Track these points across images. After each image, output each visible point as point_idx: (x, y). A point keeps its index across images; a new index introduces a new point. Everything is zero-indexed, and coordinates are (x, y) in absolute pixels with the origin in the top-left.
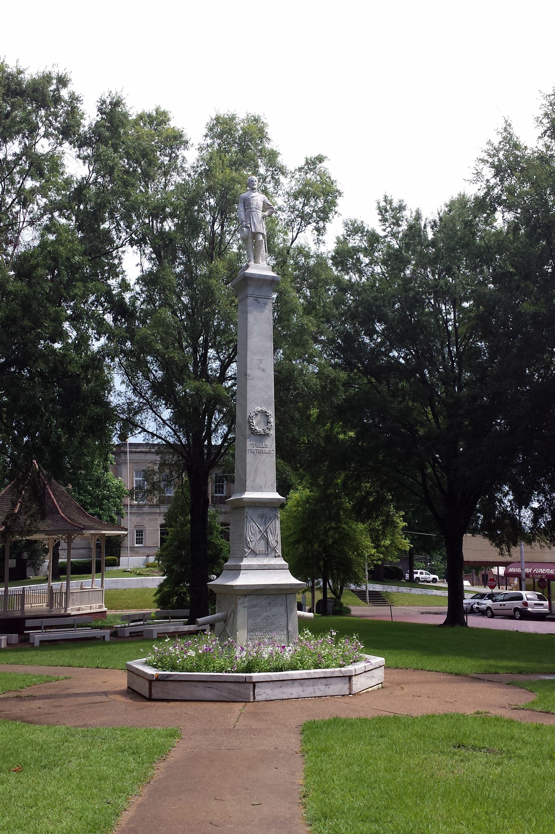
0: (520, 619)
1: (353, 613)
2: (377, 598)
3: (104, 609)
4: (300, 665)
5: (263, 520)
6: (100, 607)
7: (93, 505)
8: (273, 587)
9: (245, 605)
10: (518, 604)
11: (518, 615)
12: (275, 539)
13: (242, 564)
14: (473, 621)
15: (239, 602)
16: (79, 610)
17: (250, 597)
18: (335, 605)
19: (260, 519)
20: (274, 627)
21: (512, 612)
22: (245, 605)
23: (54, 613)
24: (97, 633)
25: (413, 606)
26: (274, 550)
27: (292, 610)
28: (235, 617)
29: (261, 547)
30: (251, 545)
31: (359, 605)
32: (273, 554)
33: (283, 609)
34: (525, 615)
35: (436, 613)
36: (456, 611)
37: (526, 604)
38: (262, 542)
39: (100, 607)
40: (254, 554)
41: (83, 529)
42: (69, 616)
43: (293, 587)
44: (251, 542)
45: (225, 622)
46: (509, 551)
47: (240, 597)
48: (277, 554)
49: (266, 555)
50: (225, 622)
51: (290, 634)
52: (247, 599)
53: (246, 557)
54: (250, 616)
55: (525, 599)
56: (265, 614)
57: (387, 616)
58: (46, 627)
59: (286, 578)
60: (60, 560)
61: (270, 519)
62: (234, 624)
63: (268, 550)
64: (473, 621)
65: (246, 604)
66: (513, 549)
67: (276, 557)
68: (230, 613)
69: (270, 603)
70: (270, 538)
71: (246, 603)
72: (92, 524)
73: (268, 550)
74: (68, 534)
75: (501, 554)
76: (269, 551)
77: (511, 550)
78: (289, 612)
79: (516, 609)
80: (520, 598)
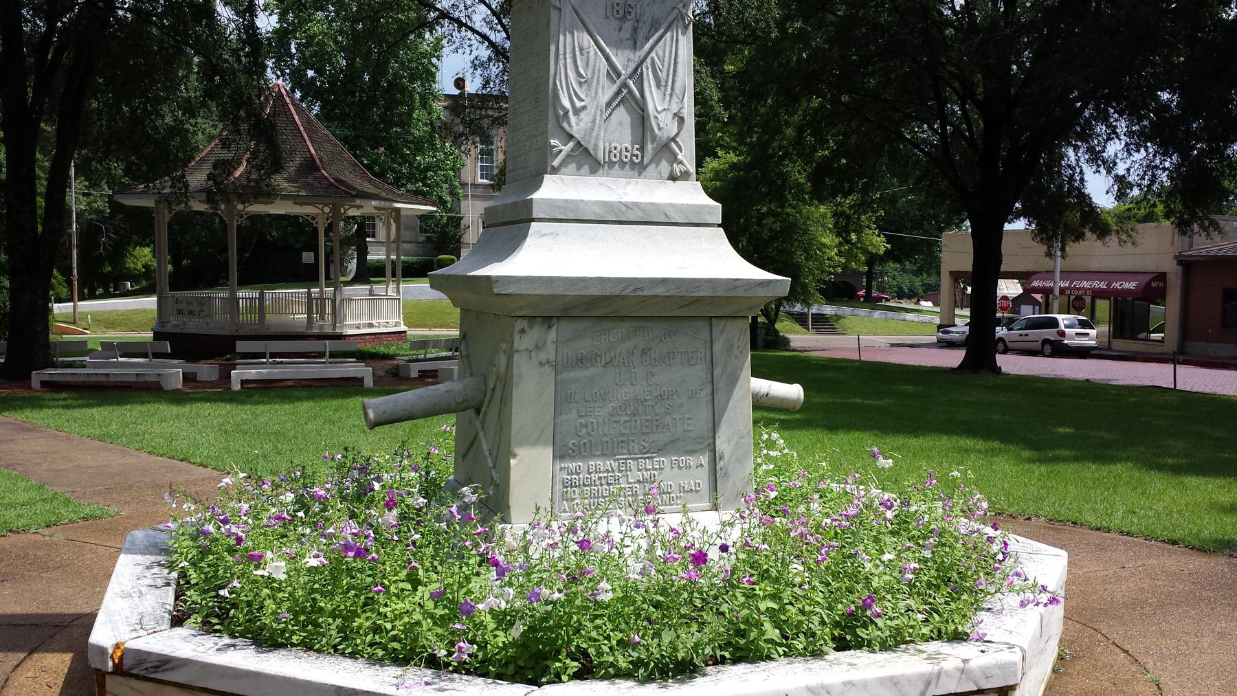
0: (1051, 356)
1: (793, 345)
2: (822, 323)
3: (403, 328)
4: (773, 634)
5: (628, 26)
6: (397, 324)
7: (411, 178)
8: (660, 291)
9: (543, 356)
10: (1050, 334)
11: (1048, 349)
12: (673, 103)
13: (536, 196)
14: (1009, 364)
15: (523, 343)
16: (371, 325)
17: (567, 328)
18: (767, 334)
19: (614, 24)
20: (662, 438)
21: (1038, 346)
22: (543, 356)
23: (316, 331)
24: (351, 368)
25: (875, 334)
26: (666, 149)
27: (733, 381)
28: (505, 401)
29: (616, 134)
30: (577, 125)
31: (797, 333)
32: (664, 167)
33: (697, 373)
34: (1059, 350)
35: (912, 346)
36: (981, 346)
37: (1062, 334)
38: (622, 115)
39: (397, 324)
40: (587, 159)
41: (356, 196)
42: (341, 337)
43: (739, 293)
44: (577, 111)
45: (478, 411)
46: (1063, 250)
47: (523, 324)
48: (678, 169)
49: (638, 168)
50: (478, 411)
51: (720, 464)
52: (553, 334)
53: (555, 171)
54: (561, 401)
55: (1062, 327)
56: (627, 392)
57: (851, 350)
58: (273, 355)
59: (714, 259)
60: (369, 257)
61: (654, 27)
62: (503, 425)
63: (642, 149)
64: (1009, 364)
65: (549, 353)
66: (1072, 248)
67: (673, 178)
68: (491, 385)
69: (644, 352)
70: (655, 100)
71: (551, 347)
72: (376, 192)
73: (642, 149)
74: (334, 205)
75: (1049, 254)
76: (647, 152)
77: (1068, 248)
78: (721, 384)
79: (1046, 341)
80: (1054, 323)
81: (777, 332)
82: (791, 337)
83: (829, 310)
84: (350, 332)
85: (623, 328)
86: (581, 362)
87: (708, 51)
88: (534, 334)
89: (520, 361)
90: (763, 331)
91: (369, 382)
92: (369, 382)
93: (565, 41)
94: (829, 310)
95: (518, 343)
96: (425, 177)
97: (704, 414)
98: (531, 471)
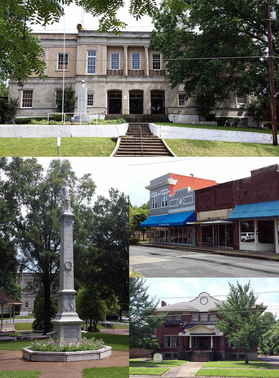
1: (100, 331)
2: (109, 326)
3: (15, 330)
6: (13, 329)
7: (10, 294)
12: (74, 306)
17: (65, 326)
18: (94, 329)
26: (73, 309)
27: (79, 330)
28: (60, 333)
29: (69, 308)
30: (65, 308)
31: (102, 328)
33: (76, 330)
38: (69, 307)
39: (13, 329)
40: (66, 311)
42: (2, 332)
49: (71, 311)
59: (78, 319)
62: (59, 335)
65: (63, 328)
70: (72, 305)
72: (10, 301)
76: (71, 310)
81: (96, 328)
82: (100, 329)
83: (109, 322)
84: (4, 331)
85: (70, 326)
86: (66, 329)
87: (76, 300)
88: (62, 326)
89: (61, 329)
90: (93, 328)
91: (16, 340)
92: (16, 340)
93: (64, 301)
94: (109, 322)
95: (61, 327)
96: (14, 294)
97: (77, 333)
98: (62, 339)
